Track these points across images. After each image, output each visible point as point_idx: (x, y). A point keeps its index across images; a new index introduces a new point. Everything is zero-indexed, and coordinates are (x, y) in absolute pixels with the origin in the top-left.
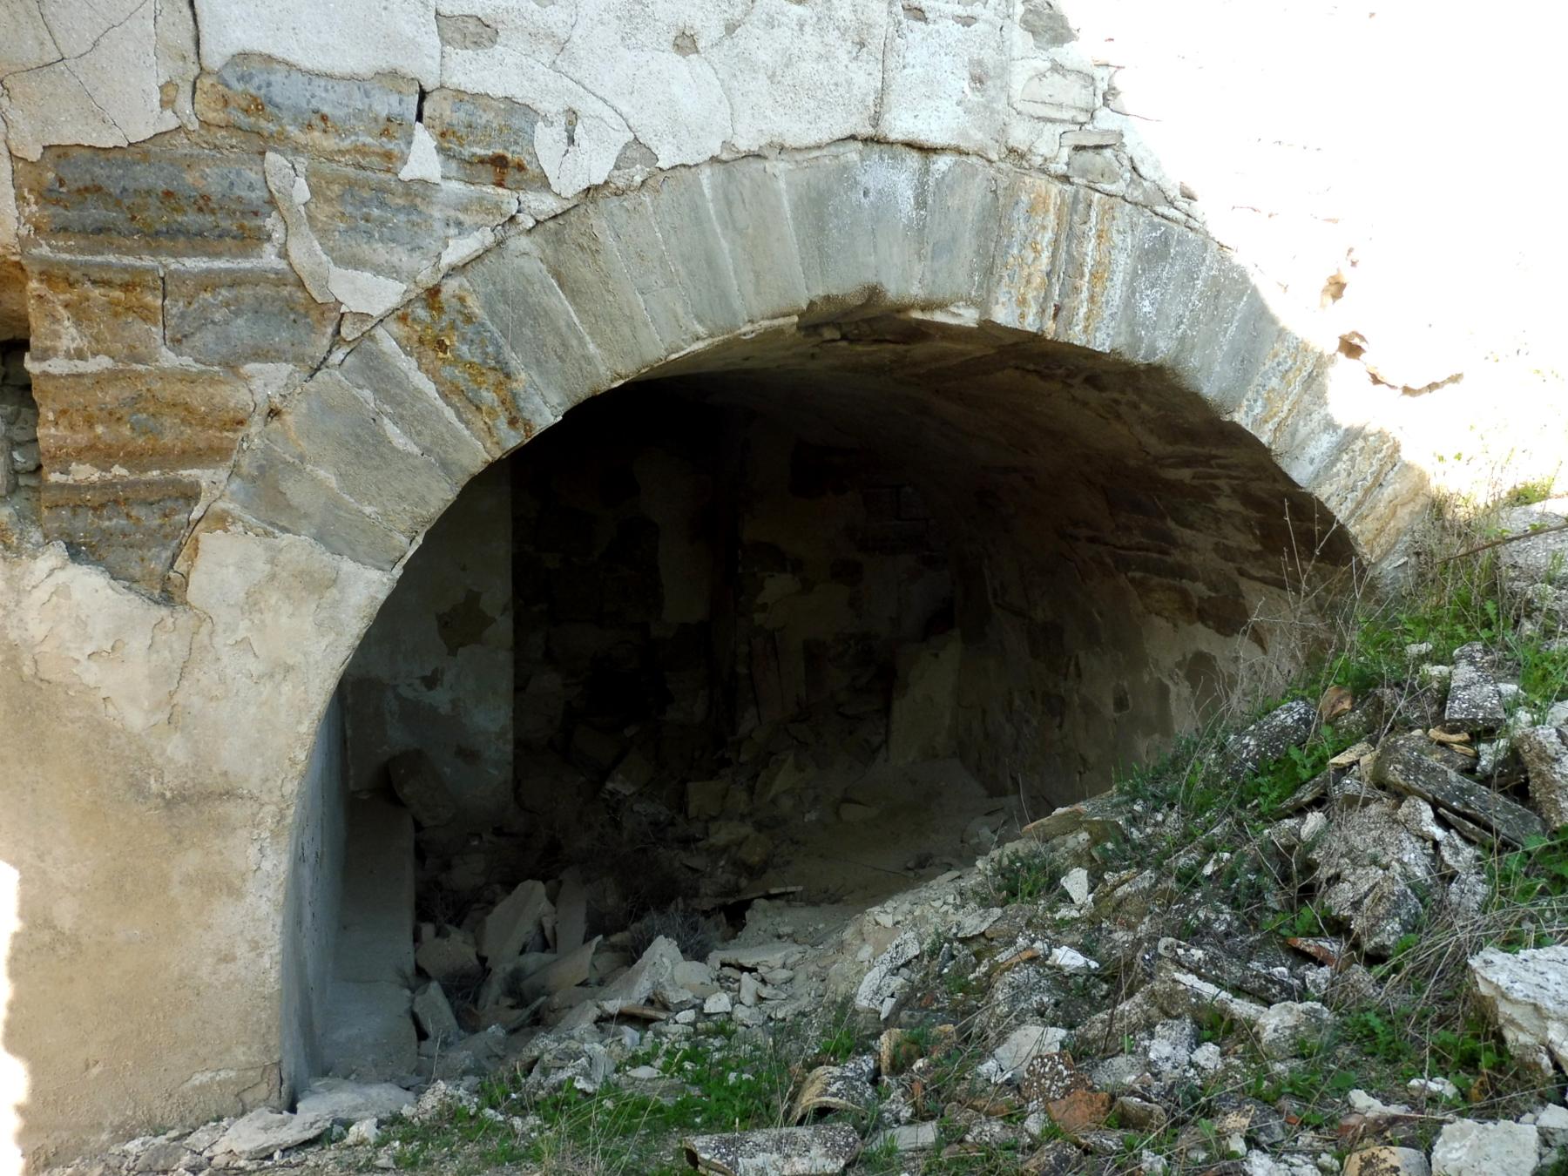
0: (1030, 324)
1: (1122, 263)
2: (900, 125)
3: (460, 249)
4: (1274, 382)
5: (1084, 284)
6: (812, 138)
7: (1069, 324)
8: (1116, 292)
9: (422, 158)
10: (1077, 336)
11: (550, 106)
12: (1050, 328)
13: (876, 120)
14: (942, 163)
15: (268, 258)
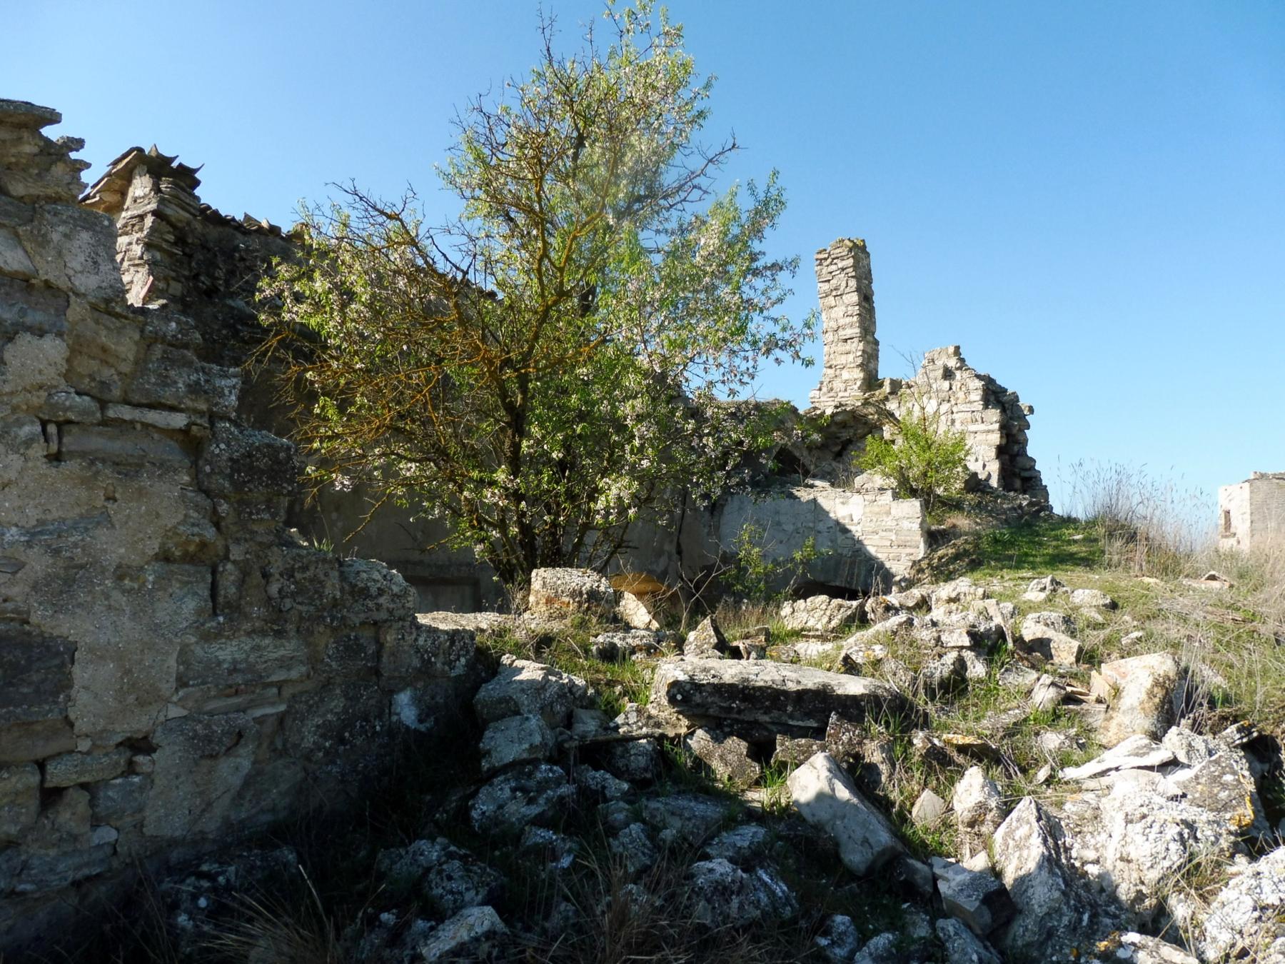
1: (863, 573)
8: (862, 578)
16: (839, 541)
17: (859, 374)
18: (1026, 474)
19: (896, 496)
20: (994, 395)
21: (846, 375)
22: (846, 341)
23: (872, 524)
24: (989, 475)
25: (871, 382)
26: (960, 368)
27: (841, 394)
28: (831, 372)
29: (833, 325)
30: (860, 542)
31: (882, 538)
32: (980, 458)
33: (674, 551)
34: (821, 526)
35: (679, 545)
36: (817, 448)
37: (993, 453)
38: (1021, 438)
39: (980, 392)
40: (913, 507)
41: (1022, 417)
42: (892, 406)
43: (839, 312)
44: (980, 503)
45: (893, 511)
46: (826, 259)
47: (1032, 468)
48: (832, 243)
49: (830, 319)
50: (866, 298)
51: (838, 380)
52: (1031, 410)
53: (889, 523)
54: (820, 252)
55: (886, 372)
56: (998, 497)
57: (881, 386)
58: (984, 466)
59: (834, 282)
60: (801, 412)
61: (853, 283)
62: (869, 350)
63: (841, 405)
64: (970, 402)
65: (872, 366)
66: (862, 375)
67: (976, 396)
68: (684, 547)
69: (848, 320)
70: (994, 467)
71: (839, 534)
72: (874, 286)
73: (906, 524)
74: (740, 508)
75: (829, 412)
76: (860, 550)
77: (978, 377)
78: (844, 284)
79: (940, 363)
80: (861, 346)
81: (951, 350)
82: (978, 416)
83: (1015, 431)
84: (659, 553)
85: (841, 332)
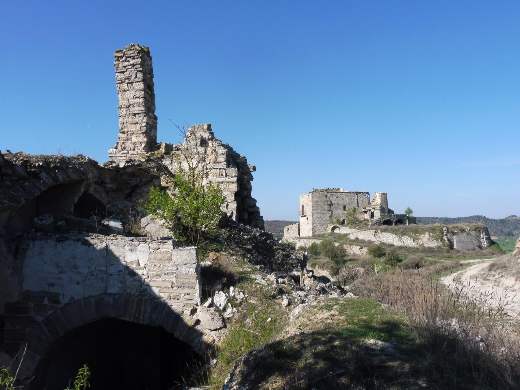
0: (132, 320)
1: (149, 309)
2: (110, 291)
3: (50, 312)
8: (148, 315)
9: (46, 301)
10: (141, 322)
12: (135, 321)
13: (105, 291)
14: (117, 296)
16: (128, 283)
17: (143, 139)
18: (251, 210)
19: (176, 245)
20: (234, 159)
21: (134, 139)
22: (134, 115)
25: (152, 145)
26: (211, 139)
27: (131, 152)
28: (124, 136)
29: (126, 103)
30: (148, 285)
34: (112, 270)
36: (113, 191)
39: (225, 156)
40: (189, 253)
41: (248, 173)
42: (166, 162)
43: (130, 94)
44: (230, 235)
45: (174, 258)
46: (122, 57)
47: (255, 205)
51: (129, 142)
52: (254, 169)
53: (170, 267)
54: (117, 52)
55: (162, 138)
57: (159, 147)
59: (127, 73)
60: (101, 164)
61: (140, 75)
62: (151, 123)
65: (152, 133)
66: (145, 140)
67: (222, 159)
71: (128, 276)
72: (155, 80)
73: (184, 269)
75: (122, 165)
76: (145, 290)
78: (134, 75)
81: (206, 127)
82: (223, 172)
83: (245, 182)
85: (131, 109)
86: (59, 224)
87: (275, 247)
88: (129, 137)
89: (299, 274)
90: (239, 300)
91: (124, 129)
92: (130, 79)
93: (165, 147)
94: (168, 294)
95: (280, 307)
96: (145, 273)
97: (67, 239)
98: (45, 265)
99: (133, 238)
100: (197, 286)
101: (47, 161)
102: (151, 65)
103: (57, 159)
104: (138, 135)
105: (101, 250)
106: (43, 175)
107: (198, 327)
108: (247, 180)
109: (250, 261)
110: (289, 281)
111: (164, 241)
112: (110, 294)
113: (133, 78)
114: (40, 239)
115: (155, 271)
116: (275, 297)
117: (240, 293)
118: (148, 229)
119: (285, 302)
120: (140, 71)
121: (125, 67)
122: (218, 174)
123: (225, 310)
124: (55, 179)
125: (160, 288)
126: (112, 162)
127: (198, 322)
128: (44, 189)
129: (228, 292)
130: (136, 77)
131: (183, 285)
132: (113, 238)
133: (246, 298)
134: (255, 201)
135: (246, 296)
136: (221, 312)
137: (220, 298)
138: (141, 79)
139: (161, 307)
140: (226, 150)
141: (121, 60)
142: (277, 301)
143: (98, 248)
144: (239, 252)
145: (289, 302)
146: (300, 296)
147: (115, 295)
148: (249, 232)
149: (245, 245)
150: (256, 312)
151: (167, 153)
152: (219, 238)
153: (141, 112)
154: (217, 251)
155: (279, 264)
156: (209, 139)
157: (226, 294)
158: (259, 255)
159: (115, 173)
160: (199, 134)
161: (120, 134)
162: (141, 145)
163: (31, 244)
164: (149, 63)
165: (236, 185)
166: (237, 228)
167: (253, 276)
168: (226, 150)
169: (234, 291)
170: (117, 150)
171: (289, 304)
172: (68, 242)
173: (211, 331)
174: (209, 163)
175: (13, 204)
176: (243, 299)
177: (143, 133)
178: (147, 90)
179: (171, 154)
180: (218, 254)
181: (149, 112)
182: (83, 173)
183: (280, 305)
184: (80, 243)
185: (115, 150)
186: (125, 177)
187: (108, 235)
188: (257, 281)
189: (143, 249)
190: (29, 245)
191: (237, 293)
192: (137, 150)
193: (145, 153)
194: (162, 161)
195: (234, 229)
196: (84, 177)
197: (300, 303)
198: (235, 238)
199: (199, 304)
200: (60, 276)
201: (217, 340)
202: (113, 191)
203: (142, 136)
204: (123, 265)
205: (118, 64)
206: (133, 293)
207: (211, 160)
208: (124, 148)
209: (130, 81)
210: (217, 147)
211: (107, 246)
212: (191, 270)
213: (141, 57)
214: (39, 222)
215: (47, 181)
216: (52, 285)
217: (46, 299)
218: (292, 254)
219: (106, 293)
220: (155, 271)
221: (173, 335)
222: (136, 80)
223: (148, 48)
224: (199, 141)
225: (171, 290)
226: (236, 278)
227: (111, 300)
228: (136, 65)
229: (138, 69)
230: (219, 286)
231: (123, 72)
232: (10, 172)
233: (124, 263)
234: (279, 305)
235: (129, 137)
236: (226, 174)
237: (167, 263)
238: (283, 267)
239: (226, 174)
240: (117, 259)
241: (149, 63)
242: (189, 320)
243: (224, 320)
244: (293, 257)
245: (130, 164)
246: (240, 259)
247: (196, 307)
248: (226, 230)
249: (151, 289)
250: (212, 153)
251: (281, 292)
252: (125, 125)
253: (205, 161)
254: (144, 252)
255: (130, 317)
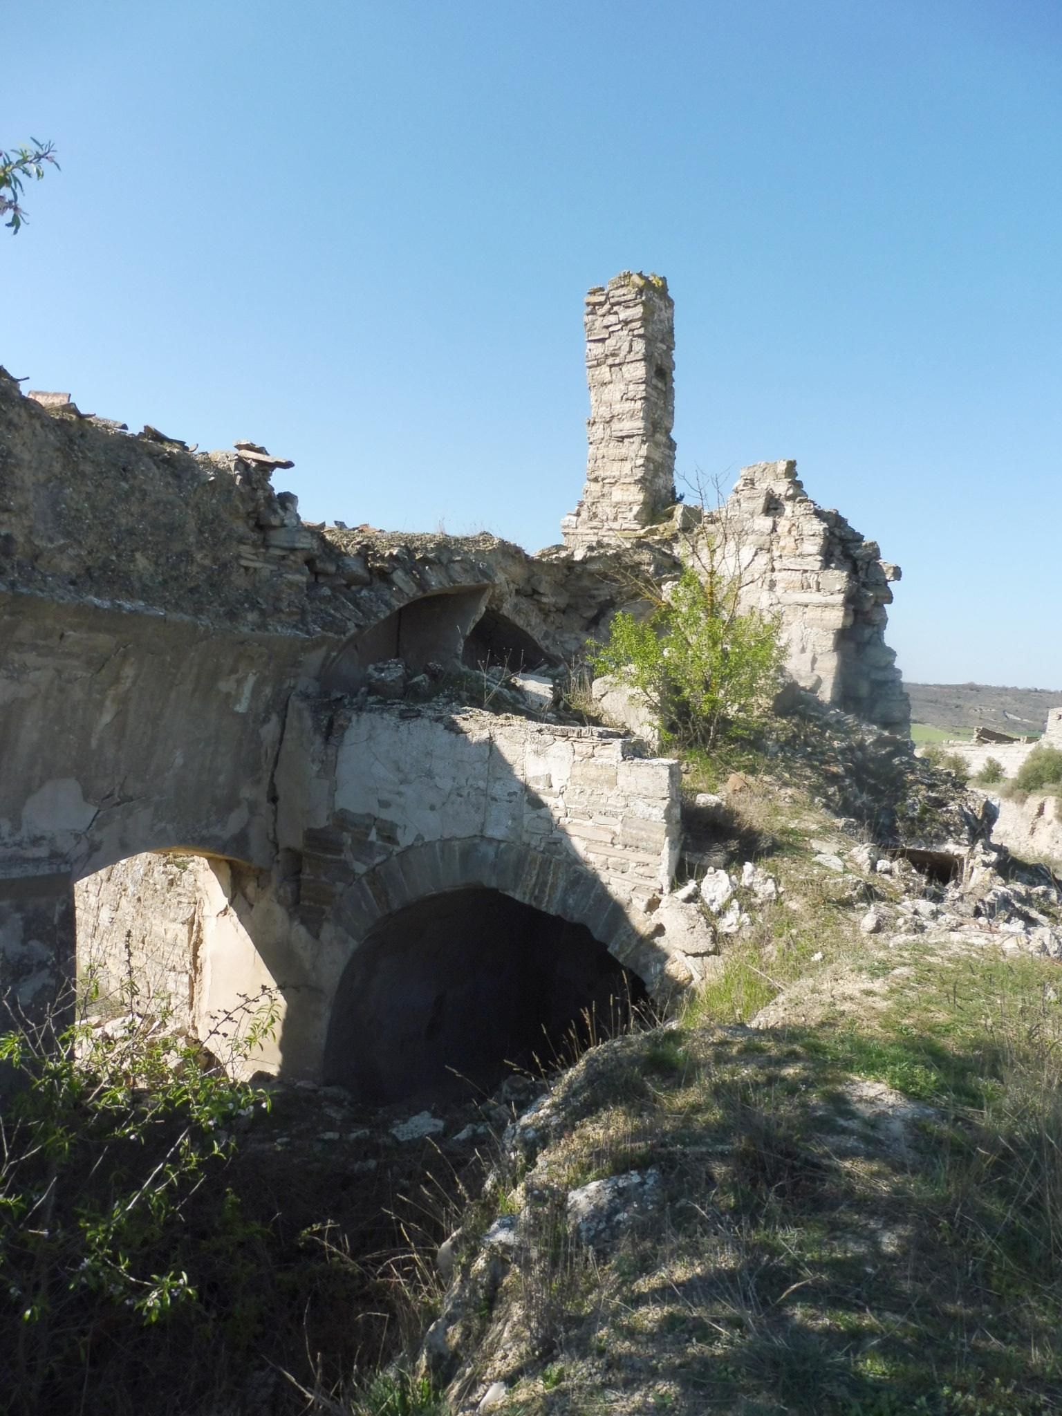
0: (526, 901)
1: (562, 884)
2: (490, 833)
3: (378, 860)
4: (624, 938)
5: (547, 890)
6: (463, 835)
7: (541, 903)
8: (558, 894)
9: (373, 836)
10: (543, 908)
11: (399, 823)
12: (534, 904)
13: (482, 831)
14: (503, 846)
15: (343, 857)
17: (636, 496)
18: (879, 676)
20: (843, 547)
21: (617, 495)
22: (621, 439)
23: (584, 799)
24: (819, 682)
25: (659, 502)
26: (790, 498)
28: (595, 487)
29: (605, 412)
31: (598, 827)
32: (809, 647)
33: (263, 798)
34: (498, 789)
35: (273, 786)
36: (558, 610)
37: (829, 641)
38: (876, 618)
39: (819, 541)
42: (679, 550)
43: (614, 392)
44: (795, 737)
45: (621, 780)
46: (601, 304)
48: (614, 278)
49: (600, 402)
50: (660, 374)
51: (606, 501)
52: (897, 573)
53: (612, 799)
54: (593, 293)
56: (827, 725)
58: (814, 661)
61: (640, 346)
62: (657, 456)
63: (600, 544)
64: (801, 555)
66: (640, 497)
67: (812, 546)
68: (280, 791)
69: (629, 406)
70: (829, 665)
72: (677, 355)
73: (640, 807)
74: (370, 738)
75: (578, 556)
76: (556, 842)
77: (819, 514)
78: (626, 347)
79: (762, 487)
80: (644, 450)
81: (782, 467)
82: (812, 579)
83: (868, 606)
84: (229, 805)
85: (616, 425)
86: (415, 680)
87: (911, 777)
88: (606, 490)
89: (962, 851)
90: (760, 895)
91: (597, 473)
92: (616, 355)
93: (683, 514)
94: (603, 858)
95: (856, 932)
96: (561, 805)
97: (419, 715)
98: (378, 764)
99: (544, 725)
100: (666, 850)
101: (409, 546)
102: (671, 319)
103: (431, 541)
104: (625, 487)
105: (479, 744)
106: (399, 576)
107: (660, 941)
108: (872, 601)
109: (826, 806)
110: (904, 870)
111: (605, 741)
112: (491, 840)
113: (623, 354)
114: (371, 711)
115: (581, 803)
116: (852, 905)
117: (766, 879)
118: (606, 703)
119: (868, 921)
120: (639, 336)
121: (607, 327)
122: (798, 584)
123: (721, 913)
124: (422, 584)
125: (588, 841)
126: (559, 548)
127: (660, 930)
128: (398, 604)
129: (739, 873)
130: (630, 351)
131: (634, 843)
132: (503, 722)
133: (779, 895)
134: (892, 653)
135: (781, 889)
136: (712, 917)
137: (716, 885)
138: (640, 356)
139: (585, 881)
140: (825, 525)
141: (600, 312)
142: (852, 915)
143: (474, 740)
144: (808, 778)
145: (878, 923)
146: (916, 913)
147: (500, 842)
148: (848, 733)
149: (828, 763)
150: (794, 931)
151: (686, 528)
152: (768, 739)
153: (635, 432)
154: (752, 770)
155: (912, 819)
156: (788, 498)
157: (734, 877)
158: (861, 791)
159: (565, 571)
160: (765, 486)
161: (588, 483)
162: (631, 510)
163: (354, 718)
164: (664, 315)
165: (842, 614)
166: (818, 719)
167: (815, 844)
168: (825, 525)
169: (753, 874)
170: (580, 519)
171: (878, 929)
172: (419, 721)
173: (687, 955)
174: (781, 557)
175: (330, 634)
176: (770, 895)
177: (636, 482)
178: (654, 381)
179: (696, 531)
180: (751, 779)
181: (655, 432)
182: (483, 573)
183: (855, 924)
184: (441, 727)
185: (575, 518)
186: (586, 582)
187: (497, 714)
188: (818, 858)
189: (560, 753)
190: (350, 720)
191: (760, 879)
192: (620, 521)
193: (638, 527)
194: (671, 549)
195: (810, 721)
196: (486, 581)
197: (908, 931)
198: (806, 744)
199: (666, 890)
200: (402, 788)
201: (697, 977)
202: (558, 610)
203: (635, 489)
204: (518, 781)
205: (593, 321)
206: (533, 843)
207: (784, 548)
208: (595, 515)
209: (617, 362)
210: (802, 518)
211: (490, 738)
212: (655, 811)
213: (643, 303)
214: (376, 674)
215: (406, 589)
216: (385, 804)
217: (374, 831)
218: (953, 799)
219: (483, 837)
220: (581, 803)
221: (607, 947)
222: (631, 357)
223: (664, 279)
224: (761, 503)
225: (609, 850)
226: (765, 844)
227: (490, 851)
228: (631, 321)
229: (636, 332)
230: (719, 858)
231: (603, 340)
232: (332, 568)
233: (522, 778)
234: (854, 925)
235: (606, 490)
236: (818, 583)
237: (606, 790)
238: (922, 830)
239: (818, 583)
240: (509, 768)
241: (664, 315)
242: (642, 922)
243: (716, 937)
244: (953, 806)
245: (595, 554)
246: (803, 796)
247: (660, 896)
248: (790, 722)
249: (569, 841)
250: (790, 531)
251: (870, 894)
252: (599, 462)
253: (769, 550)
254: (563, 759)
255: (525, 893)
